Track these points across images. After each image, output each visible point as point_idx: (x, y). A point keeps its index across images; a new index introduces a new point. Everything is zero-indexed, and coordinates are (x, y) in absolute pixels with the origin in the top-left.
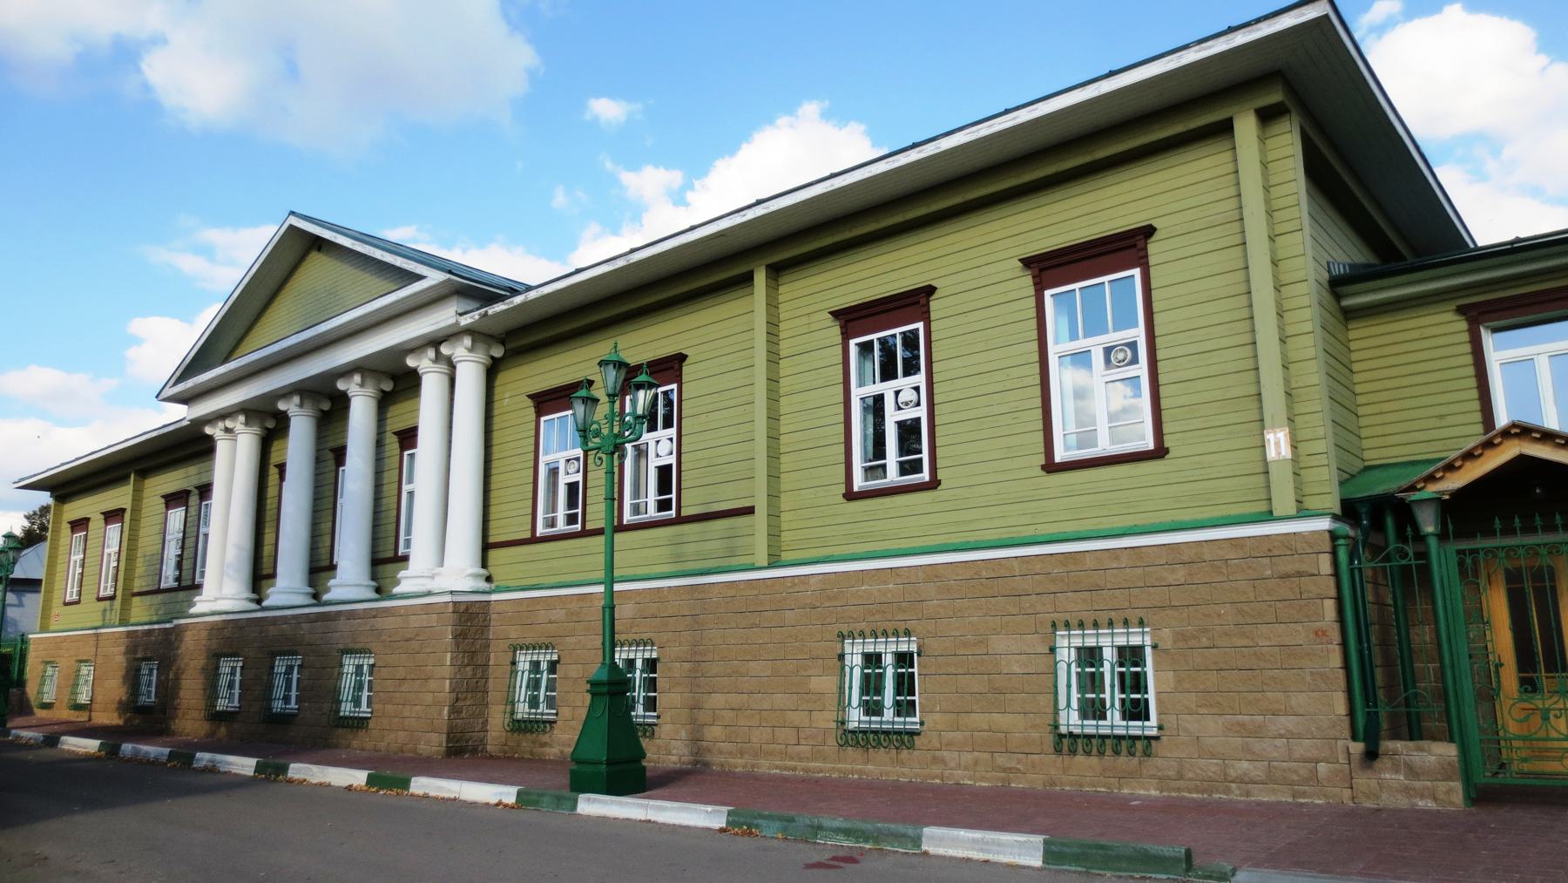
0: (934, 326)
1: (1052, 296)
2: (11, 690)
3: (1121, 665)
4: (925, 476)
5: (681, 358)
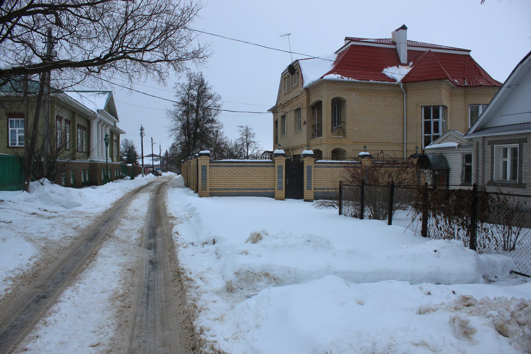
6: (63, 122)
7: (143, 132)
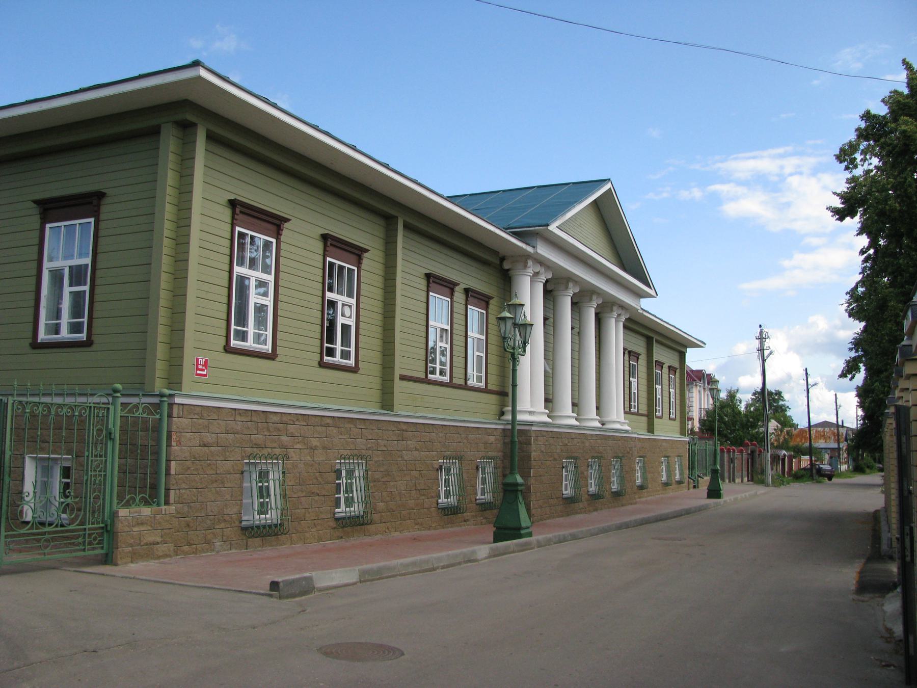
0: (102, 225)
1: (50, 228)
2: (29, 516)
3: (260, 482)
4: (83, 336)
5: (100, 195)
6: (665, 370)
7: (766, 345)
